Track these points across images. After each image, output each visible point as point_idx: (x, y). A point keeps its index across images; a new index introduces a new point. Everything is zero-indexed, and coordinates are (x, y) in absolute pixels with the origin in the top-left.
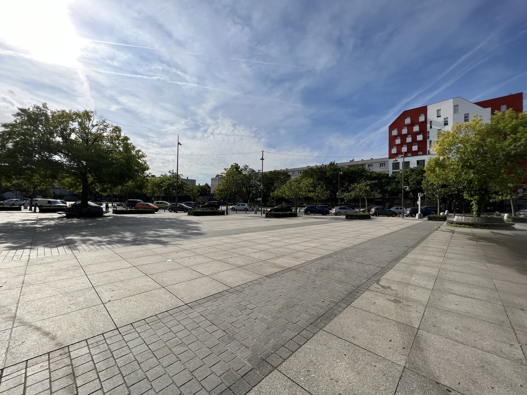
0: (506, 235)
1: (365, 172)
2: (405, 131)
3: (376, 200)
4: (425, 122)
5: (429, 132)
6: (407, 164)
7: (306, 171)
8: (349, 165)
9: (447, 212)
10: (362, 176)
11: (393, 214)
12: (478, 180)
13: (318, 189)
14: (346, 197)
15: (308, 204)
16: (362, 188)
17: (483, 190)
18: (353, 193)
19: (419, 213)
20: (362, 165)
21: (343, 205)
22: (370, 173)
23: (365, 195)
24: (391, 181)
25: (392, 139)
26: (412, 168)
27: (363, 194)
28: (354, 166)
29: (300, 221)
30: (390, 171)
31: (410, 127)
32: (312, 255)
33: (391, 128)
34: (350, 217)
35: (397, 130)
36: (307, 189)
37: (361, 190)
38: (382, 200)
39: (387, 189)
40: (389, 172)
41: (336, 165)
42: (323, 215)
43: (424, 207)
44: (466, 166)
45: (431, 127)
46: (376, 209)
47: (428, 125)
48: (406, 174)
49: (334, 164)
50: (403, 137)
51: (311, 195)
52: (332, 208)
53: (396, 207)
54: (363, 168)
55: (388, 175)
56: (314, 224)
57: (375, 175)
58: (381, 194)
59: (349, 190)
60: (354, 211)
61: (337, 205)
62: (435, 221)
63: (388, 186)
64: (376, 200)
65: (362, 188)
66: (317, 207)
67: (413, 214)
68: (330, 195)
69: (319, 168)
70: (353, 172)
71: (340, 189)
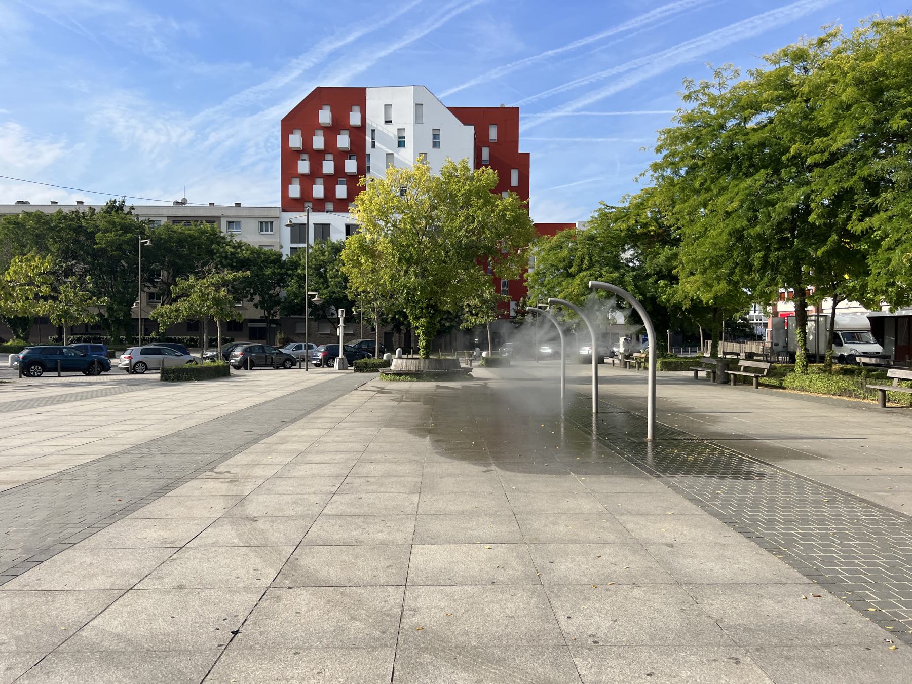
0: (452, 388)
1: (218, 243)
2: (318, 142)
3: (250, 325)
4: (362, 128)
5: (369, 155)
6: (323, 230)
7: (17, 224)
8: (170, 214)
9: (399, 351)
10: (211, 253)
11: (285, 361)
12: (421, 287)
13: (67, 291)
14: (162, 316)
15: (25, 339)
16: (208, 294)
17: (432, 307)
18: (183, 305)
19: (341, 356)
20: (212, 220)
21: (153, 340)
22: (234, 247)
23: (217, 313)
24: (287, 274)
25: (289, 157)
26: (336, 242)
27: (209, 308)
28: (187, 220)
29: (8, 395)
30: (283, 245)
31: (331, 132)
32: (81, 458)
33: (289, 124)
34: (172, 376)
35: (302, 136)
36: (31, 290)
37: (203, 297)
38: (264, 325)
39: (278, 295)
40: (281, 247)
41: (130, 213)
42: (87, 375)
43: (353, 344)
44: (405, 258)
45: (373, 146)
46: (245, 351)
47: (368, 139)
48: (322, 258)
49: (121, 207)
50: (317, 157)
51: (42, 308)
52: (117, 353)
53: (296, 344)
54: (213, 229)
55: (281, 256)
56: (64, 402)
57: (246, 254)
58: (262, 308)
59: (173, 296)
60: (186, 358)
61: (134, 342)
62: (368, 372)
63: (280, 287)
64: (250, 325)
65: (208, 294)
66: (64, 350)
67: (327, 361)
68: (110, 309)
69: (65, 217)
70: (182, 241)
71: (142, 291)
